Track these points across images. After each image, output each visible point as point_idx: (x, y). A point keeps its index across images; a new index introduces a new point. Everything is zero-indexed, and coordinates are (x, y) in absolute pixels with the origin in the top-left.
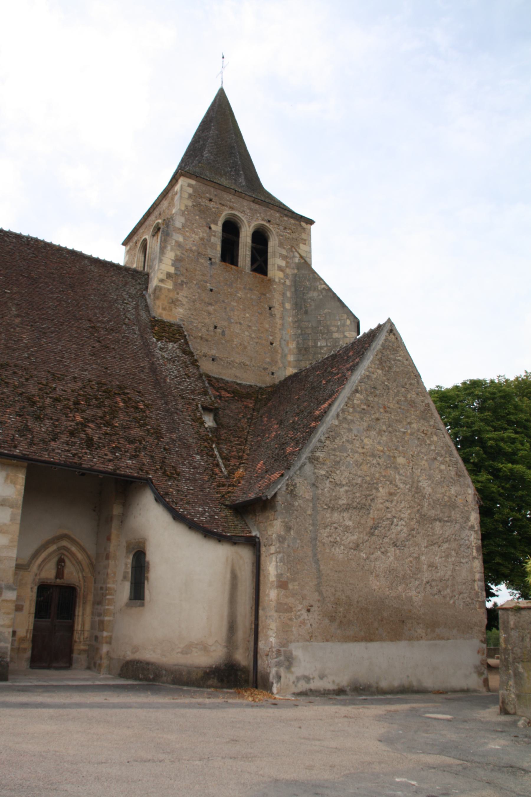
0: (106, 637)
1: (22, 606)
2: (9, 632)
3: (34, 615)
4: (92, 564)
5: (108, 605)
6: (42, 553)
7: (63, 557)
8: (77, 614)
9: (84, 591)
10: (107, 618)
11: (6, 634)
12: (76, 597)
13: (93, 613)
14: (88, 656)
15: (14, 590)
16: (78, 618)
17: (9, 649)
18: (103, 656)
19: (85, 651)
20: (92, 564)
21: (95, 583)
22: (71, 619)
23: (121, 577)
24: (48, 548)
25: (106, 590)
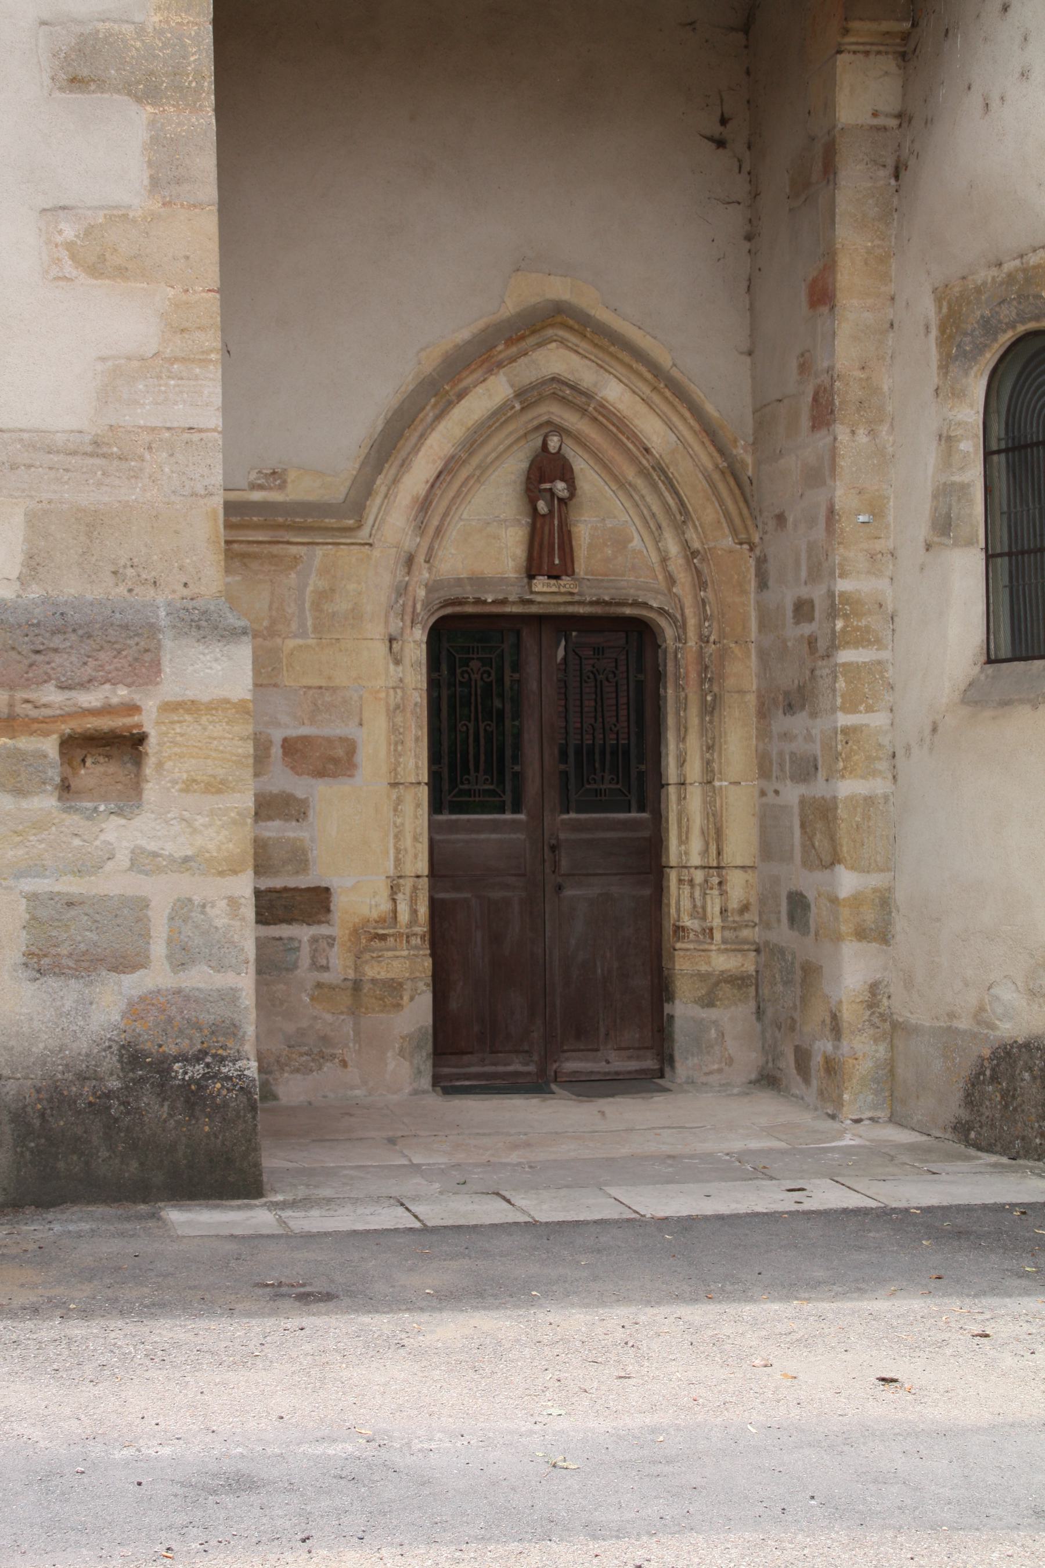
0: (857, 900)
1: (351, 747)
2: (233, 902)
3: (423, 793)
4: (732, 472)
5: (851, 708)
6: (432, 427)
7: (554, 443)
8: (671, 773)
9: (704, 639)
10: (847, 788)
11: (219, 916)
12: (659, 677)
13: (764, 767)
14: (759, 1013)
15: (233, 634)
16: (682, 799)
17: (248, 999)
18: (848, 1014)
19: (738, 981)
20: (732, 472)
21: (763, 585)
22: (642, 809)
23: (922, 530)
24: (461, 396)
25: (833, 613)
